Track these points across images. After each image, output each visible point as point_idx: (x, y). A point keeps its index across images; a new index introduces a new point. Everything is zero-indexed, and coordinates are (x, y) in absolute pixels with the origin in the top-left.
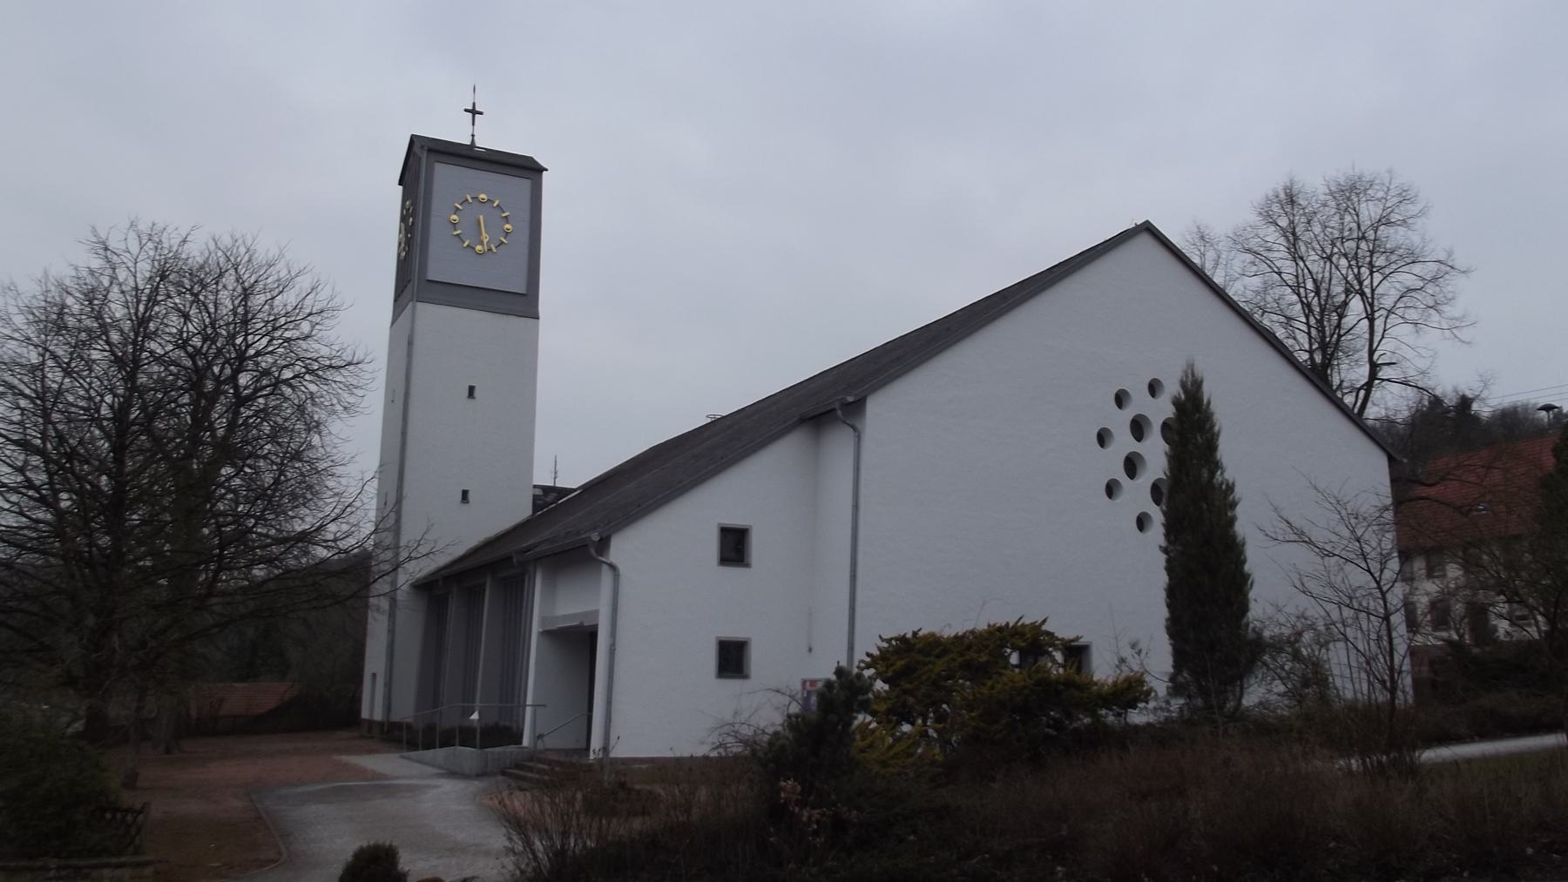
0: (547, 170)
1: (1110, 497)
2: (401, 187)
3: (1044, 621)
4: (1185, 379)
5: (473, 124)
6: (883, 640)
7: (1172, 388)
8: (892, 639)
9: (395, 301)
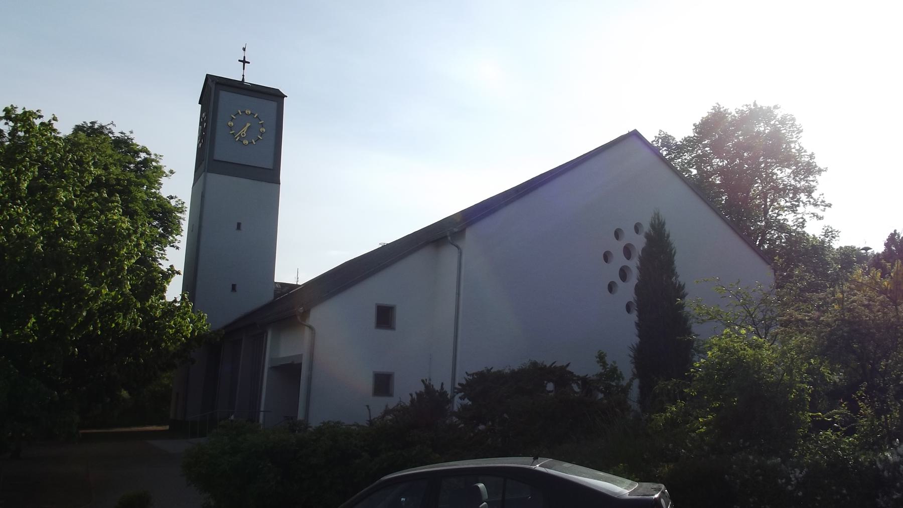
0: (286, 97)
1: (606, 262)
2: (200, 105)
3: (568, 365)
4: (653, 222)
5: (244, 69)
6: (468, 375)
7: (646, 227)
8: (474, 374)
9: (195, 172)
